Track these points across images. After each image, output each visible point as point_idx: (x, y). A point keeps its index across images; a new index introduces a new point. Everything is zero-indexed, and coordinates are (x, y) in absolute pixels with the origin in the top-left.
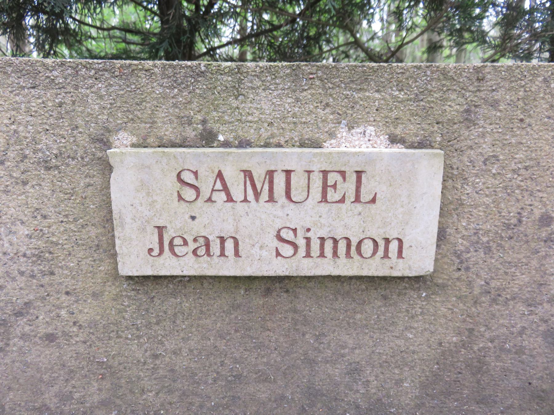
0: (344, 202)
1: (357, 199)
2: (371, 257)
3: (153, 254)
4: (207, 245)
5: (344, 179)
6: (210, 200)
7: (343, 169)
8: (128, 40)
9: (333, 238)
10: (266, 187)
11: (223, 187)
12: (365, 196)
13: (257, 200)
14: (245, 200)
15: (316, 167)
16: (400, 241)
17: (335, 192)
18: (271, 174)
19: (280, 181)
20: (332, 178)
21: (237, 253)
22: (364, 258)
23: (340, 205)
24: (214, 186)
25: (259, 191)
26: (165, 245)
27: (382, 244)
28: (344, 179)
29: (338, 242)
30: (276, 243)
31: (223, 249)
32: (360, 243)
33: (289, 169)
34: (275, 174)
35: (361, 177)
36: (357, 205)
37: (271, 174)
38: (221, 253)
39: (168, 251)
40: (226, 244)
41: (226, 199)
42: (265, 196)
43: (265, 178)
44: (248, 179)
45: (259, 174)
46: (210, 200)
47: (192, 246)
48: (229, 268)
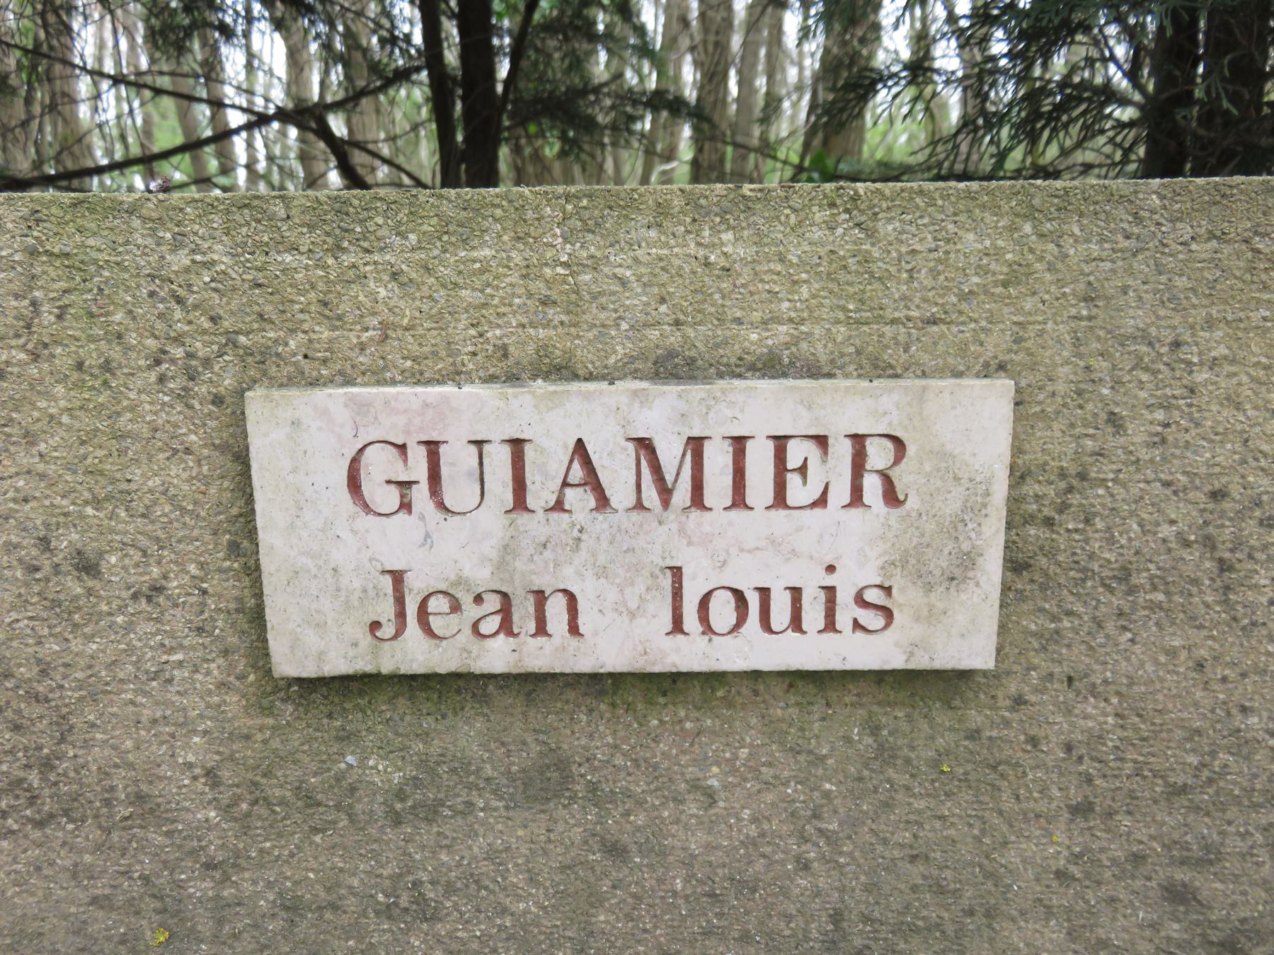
0: (825, 506)
2: (729, 633)
4: (506, 611)
6: (559, 506)
9: (565, 591)
13: (666, 503)
14: (639, 506)
16: (572, 599)
17: (805, 483)
19: (718, 460)
20: (796, 453)
21: (574, 629)
22: (367, 508)
23: (818, 511)
27: (753, 600)
29: (546, 599)
37: (696, 445)
38: (537, 628)
43: (684, 455)
45: (670, 452)
47: (471, 611)
48: (540, 655)
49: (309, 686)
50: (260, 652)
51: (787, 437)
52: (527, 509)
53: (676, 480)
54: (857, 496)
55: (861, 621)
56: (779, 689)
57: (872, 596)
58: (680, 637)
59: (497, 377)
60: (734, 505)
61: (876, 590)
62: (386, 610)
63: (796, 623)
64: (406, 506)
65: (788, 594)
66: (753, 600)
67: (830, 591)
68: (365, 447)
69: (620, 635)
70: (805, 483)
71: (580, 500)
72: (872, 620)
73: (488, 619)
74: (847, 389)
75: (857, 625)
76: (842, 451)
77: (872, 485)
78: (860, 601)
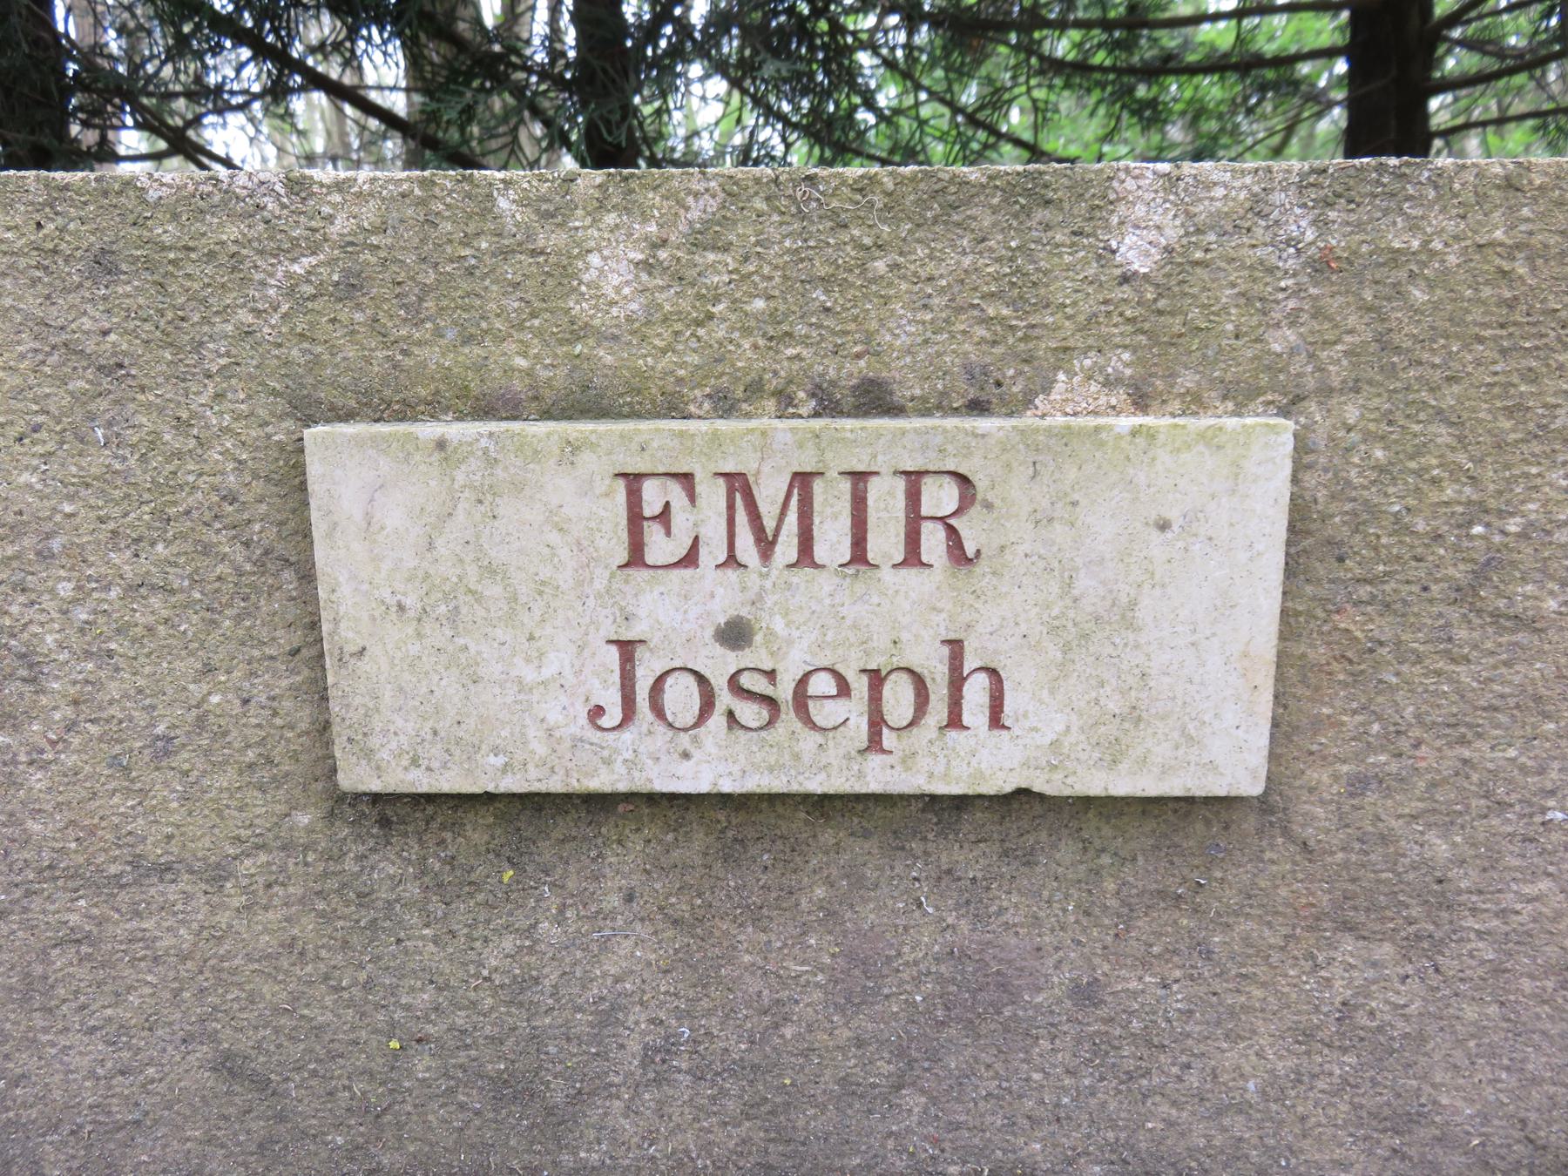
3: (605, 722)
5: (692, 497)
10: (792, 518)
11: (918, 533)
14: (732, 560)
17: (668, 533)
18: (803, 481)
20: (653, 496)
21: (996, 721)
26: (638, 699)
28: (692, 497)
29: (965, 679)
32: (659, 682)
33: (861, 468)
34: (818, 486)
35: (639, 490)
37: (803, 481)
39: (792, 714)
40: (968, 689)
42: (787, 549)
44: (738, 496)
45: (770, 492)
48: (980, 762)
49: (391, 812)
51: (920, 474)
52: (867, 563)
54: (912, 556)
55: (737, 714)
56: (665, 802)
59: (589, 411)
60: (904, 563)
61: (757, 676)
62: (612, 699)
70: (668, 533)
74: (359, 442)
76: (713, 495)
77: (933, 541)
78: (770, 702)
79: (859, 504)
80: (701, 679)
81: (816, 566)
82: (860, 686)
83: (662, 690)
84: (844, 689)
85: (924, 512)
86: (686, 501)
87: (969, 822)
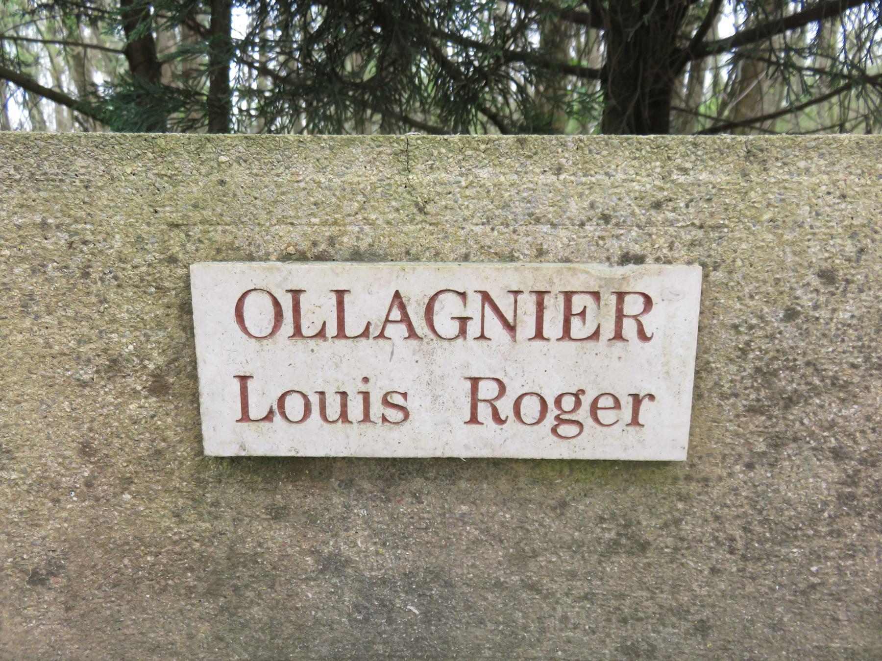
1: (341, 333)
6: (382, 335)
7: (596, 289)
8: (56, 83)
12: (353, 327)
15: (560, 286)
23: (590, 344)
24: (388, 315)
25: (512, 324)
27: (315, 400)
30: (410, 405)
31: (344, 406)
33: (516, 289)
36: (567, 344)
41: (407, 335)
42: (527, 327)
46: (382, 335)
50: (200, 451)
53: (515, 316)
54: (618, 336)
57: (398, 400)
58: (368, 424)
63: (344, 416)
64: (463, 332)
65: (317, 396)
66: (315, 400)
67: (366, 395)
68: (437, 294)
69: (437, 431)
71: (397, 331)
72: (395, 415)
73: (260, 418)
75: (384, 419)
76: (475, 301)
79: (540, 308)
80: (304, 396)
81: (486, 338)
82: (627, 404)
83: (520, 404)
84: (617, 405)
85: (574, 313)
86: (595, 306)
87: (453, 477)
